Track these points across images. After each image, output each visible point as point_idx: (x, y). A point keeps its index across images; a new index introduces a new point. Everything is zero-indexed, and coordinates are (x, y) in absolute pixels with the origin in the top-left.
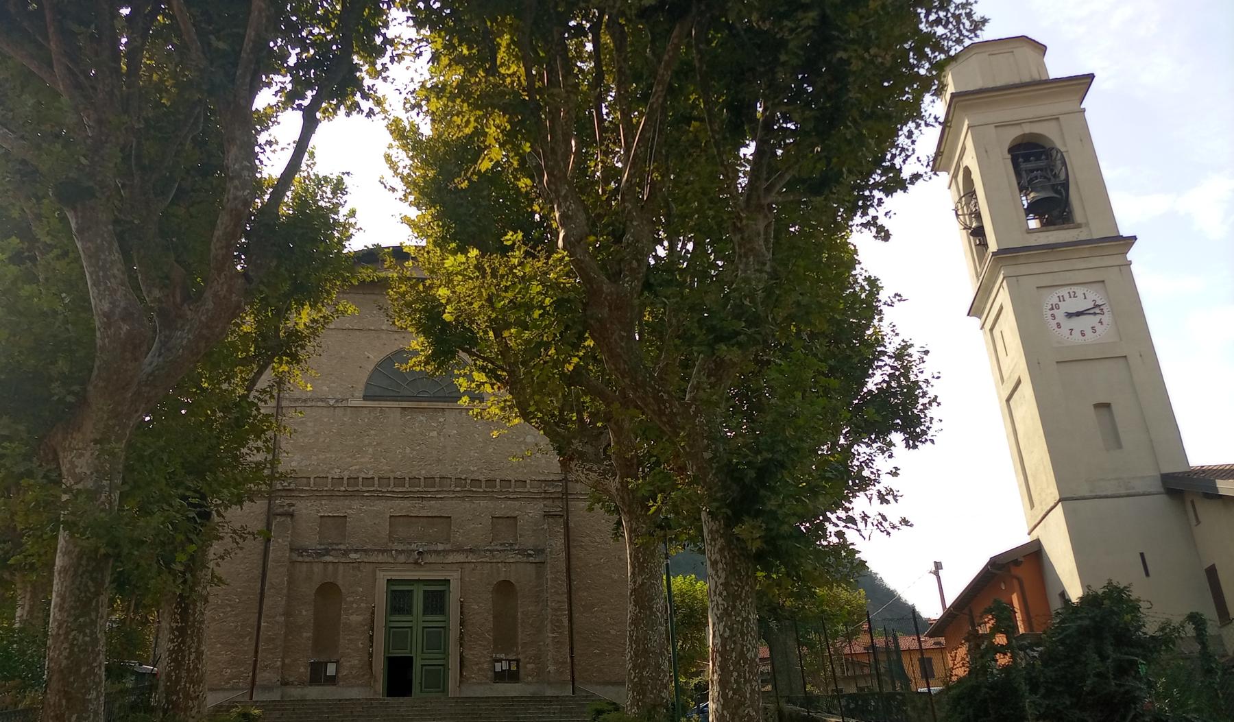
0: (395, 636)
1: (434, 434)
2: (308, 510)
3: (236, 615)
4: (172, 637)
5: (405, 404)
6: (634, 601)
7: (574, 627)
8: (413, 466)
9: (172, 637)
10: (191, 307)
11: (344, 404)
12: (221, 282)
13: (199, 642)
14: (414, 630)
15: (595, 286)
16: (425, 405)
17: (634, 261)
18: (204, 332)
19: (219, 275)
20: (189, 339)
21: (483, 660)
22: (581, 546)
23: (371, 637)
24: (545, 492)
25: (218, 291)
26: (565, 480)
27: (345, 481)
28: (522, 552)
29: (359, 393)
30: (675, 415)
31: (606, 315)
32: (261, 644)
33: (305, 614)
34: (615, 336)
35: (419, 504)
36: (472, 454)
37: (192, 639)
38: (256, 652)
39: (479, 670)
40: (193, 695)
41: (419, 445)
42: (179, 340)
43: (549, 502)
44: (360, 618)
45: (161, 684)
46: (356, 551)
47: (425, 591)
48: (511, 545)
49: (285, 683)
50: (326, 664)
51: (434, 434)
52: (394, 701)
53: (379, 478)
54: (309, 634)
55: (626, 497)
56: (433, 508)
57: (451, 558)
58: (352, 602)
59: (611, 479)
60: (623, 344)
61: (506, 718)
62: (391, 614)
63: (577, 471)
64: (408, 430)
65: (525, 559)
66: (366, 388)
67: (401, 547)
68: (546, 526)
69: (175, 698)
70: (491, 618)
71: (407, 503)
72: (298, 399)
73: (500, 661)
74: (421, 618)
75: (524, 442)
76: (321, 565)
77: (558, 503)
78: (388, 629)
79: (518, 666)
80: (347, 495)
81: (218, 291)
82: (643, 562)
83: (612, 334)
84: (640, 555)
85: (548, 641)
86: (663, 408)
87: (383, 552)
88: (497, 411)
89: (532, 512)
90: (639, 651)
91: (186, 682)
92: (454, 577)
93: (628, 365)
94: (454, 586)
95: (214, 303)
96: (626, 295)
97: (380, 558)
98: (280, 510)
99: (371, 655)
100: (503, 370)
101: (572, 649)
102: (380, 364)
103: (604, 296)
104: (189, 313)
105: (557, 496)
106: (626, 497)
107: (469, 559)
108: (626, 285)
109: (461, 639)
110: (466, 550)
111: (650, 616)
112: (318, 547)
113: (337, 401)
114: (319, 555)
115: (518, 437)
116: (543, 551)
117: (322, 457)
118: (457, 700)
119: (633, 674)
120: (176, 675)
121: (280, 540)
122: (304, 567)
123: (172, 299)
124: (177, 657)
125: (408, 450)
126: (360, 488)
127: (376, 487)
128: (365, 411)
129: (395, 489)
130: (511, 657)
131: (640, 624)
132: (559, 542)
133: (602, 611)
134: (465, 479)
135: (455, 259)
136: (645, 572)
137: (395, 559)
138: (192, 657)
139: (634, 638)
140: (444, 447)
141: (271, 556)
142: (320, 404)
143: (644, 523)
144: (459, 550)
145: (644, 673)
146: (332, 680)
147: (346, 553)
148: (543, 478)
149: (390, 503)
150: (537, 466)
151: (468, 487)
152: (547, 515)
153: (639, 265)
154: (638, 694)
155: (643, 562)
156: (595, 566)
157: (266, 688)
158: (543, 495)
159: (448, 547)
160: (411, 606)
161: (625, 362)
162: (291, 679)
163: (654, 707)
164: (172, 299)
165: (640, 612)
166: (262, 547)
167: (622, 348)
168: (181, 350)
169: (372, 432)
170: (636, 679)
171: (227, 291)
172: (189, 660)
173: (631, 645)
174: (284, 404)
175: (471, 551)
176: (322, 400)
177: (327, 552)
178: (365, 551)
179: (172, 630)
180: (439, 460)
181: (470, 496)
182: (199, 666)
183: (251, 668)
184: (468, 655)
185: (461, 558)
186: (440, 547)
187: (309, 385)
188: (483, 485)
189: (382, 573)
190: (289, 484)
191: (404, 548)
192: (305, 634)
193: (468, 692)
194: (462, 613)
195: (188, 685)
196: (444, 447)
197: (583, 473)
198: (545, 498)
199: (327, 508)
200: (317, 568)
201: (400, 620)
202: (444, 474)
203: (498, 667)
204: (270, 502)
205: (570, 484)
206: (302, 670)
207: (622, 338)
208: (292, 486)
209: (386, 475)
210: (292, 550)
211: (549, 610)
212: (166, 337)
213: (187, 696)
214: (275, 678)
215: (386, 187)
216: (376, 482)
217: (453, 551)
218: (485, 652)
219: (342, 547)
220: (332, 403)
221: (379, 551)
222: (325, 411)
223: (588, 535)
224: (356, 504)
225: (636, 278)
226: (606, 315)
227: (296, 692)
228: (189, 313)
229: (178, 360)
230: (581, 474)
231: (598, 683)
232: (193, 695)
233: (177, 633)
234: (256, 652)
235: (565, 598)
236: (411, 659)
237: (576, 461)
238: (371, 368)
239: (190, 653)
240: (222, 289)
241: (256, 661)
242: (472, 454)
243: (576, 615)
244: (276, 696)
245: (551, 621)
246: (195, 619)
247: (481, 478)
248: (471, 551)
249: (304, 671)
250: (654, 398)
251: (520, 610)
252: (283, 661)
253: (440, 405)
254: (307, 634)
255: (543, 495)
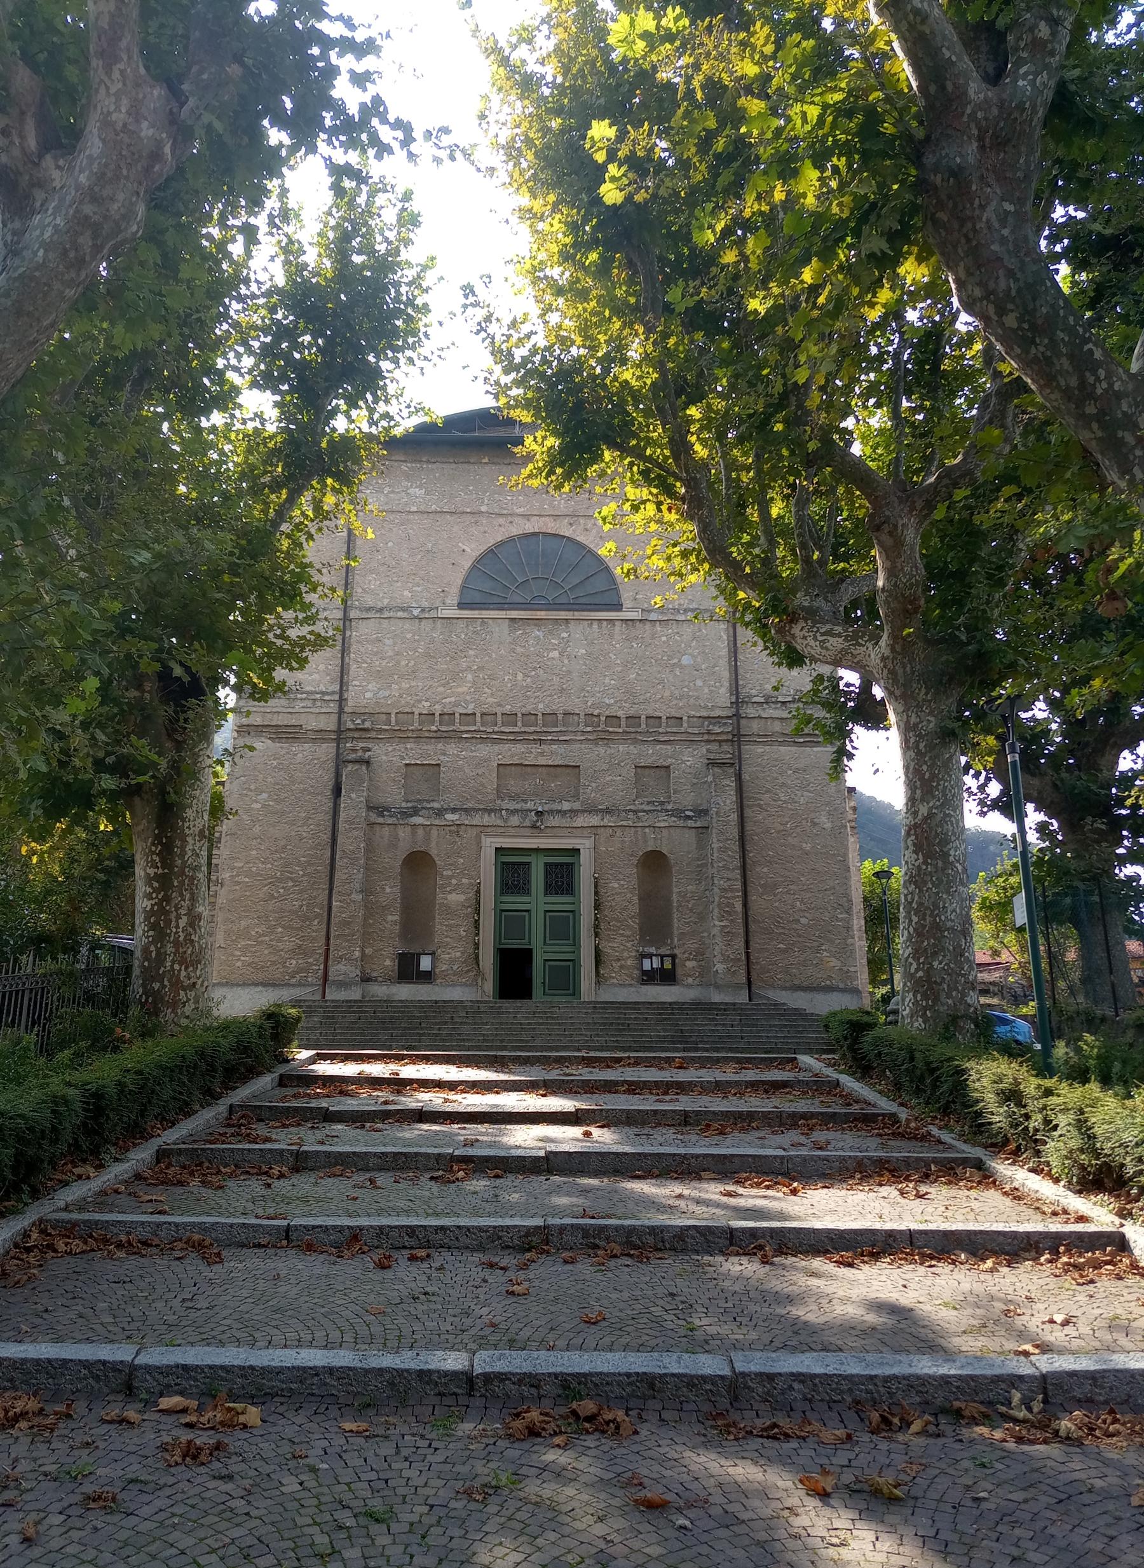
0: (508, 922)
1: (555, 654)
2: (385, 754)
3: (300, 892)
4: (149, 890)
5: (514, 614)
6: (915, 845)
7: (750, 913)
8: (528, 697)
9: (149, 890)
10: (61, 162)
11: (433, 614)
12: (113, 90)
13: (193, 899)
14: (533, 914)
15: (950, 87)
16: (542, 614)
17: (1043, 23)
18: (88, 209)
19: (109, 73)
20: (56, 226)
21: (625, 954)
22: (759, 806)
23: (477, 922)
24: (709, 733)
25: (109, 113)
26: (737, 716)
27: (437, 718)
28: (678, 813)
29: (453, 599)
30: (1118, 396)
31: (971, 159)
32: (333, 928)
33: (391, 890)
34: (989, 214)
35: (536, 749)
36: (607, 680)
37: (181, 895)
38: (328, 939)
39: (621, 967)
40: (187, 983)
41: (535, 669)
42: (38, 232)
43: (714, 747)
44: (461, 898)
45: (136, 963)
46: (454, 810)
47: (546, 864)
48: (662, 803)
49: (366, 979)
50: (419, 955)
51: (555, 654)
52: (508, 1005)
53: (483, 714)
54: (396, 918)
55: (900, 671)
56: (556, 754)
57: (580, 821)
58: (450, 877)
59: (869, 645)
60: (1006, 232)
61: (665, 1030)
62: (502, 893)
63: (805, 638)
64: (519, 650)
65: (681, 823)
66: (462, 593)
67: (513, 806)
68: (710, 779)
69: (156, 986)
70: (636, 899)
71: (520, 748)
72: (369, 609)
73: (650, 956)
74: (542, 899)
75: (679, 665)
76: (408, 829)
77: (726, 747)
78: (500, 913)
79: (673, 964)
80: (439, 736)
81: (109, 113)
82: (931, 779)
83: (982, 207)
84: (925, 768)
85: (715, 931)
86: (1091, 380)
87: (489, 811)
88: (661, 564)
89: (690, 759)
90: (924, 926)
91: (173, 962)
92: (585, 845)
93: (1017, 280)
94: (586, 859)
95: (103, 141)
96: (1021, 108)
97: (486, 820)
98: (352, 756)
99: (477, 946)
100: (677, 478)
101: (747, 942)
102: (480, 560)
103: (969, 111)
104: (56, 174)
105: (724, 737)
106: (900, 671)
107: (606, 822)
108: (1021, 83)
109: (596, 926)
110: (601, 811)
111: (943, 869)
112: (404, 805)
113: (423, 610)
114: (405, 814)
115: (670, 658)
116: (706, 812)
117: (404, 685)
118: (598, 1006)
119: (914, 966)
120: (158, 950)
121: (353, 796)
122: (386, 831)
123: (17, 141)
124: (159, 921)
125: (520, 676)
126: (457, 727)
127: (478, 726)
128: (461, 624)
129: (503, 729)
130: (663, 951)
131: (925, 883)
132: (729, 800)
133: (788, 893)
134: (598, 716)
135: (632, 23)
136: (934, 797)
137: (506, 821)
138: (183, 922)
139: (914, 905)
140: (569, 672)
141: (342, 815)
142: (400, 614)
143: (931, 713)
144: (592, 810)
145: (935, 964)
146: (427, 977)
147: (440, 813)
148: (705, 714)
149: (497, 748)
150: (698, 698)
151: (602, 726)
152: (712, 763)
153: (1054, 34)
154: (925, 997)
155: (931, 779)
156: (778, 832)
157: (342, 985)
158: (706, 737)
159: (577, 806)
160: (528, 882)
161: (1011, 274)
162: (375, 974)
163: (954, 1019)
164: (17, 141)
165: (925, 863)
166: (331, 805)
167: (1003, 241)
168: (41, 253)
169: (471, 652)
170: (920, 974)
171: (129, 113)
172: (177, 927)
173: (908, 916)
174: (353, 614)
175: (608, 811)
176: (403, 609)
177: (416, 812)
178: (466, 810)
179: (149, 880)
180: (562, 691)
181: (605, 738)
182: (195, 938)
183: (322, 959)
184: (607, 948)
185: (595, 820)
186: (566, 806)
187: (369, 530)
188: (623, 722)
189: (489, 840)
190: (363, 721)
191: (518, 806)
192: (390, 918)
193: (606, 995)
194: (596, 893)
195: (177, 967)
196: (569, 672)
197: (815, 639)
198: (708, 741)
199: (414, 753)
200: (403, 833)
201: (515, 901)
202: (569, 709)
203: (647, 964)
204: (338, 748)
205: (743, 722)
206: (388, 963)
207: (1004, 217)
208: (367, 725)
209: (493, 710)
210: (369, 808)
211: (716, 890)
212: (14, 233)
213: (177, 984)
214: (353, 972)
215: (479, 170)
216: (478, 719)
217: (583, 811)
218: (629, 945)
219: (436, 805)
220: (416, 612)
221: (485, 810)
222: (408, 625)
223: (768, 791)
224: (452, 749)
225: (1046, 67)
226: (971, 159)
227: (380, 991)
228: (56, 174)
229: (37, 274)
230: (812, 643)
231: (785, 988)
232: (187, 983)
233: (156, 885)
234: (328, 939)
235: (737, 874)
236: (529, 952)
237: (801, 623)
238: (467, 565)
239: (178, 917)
240: (118, 109)
241: (327, 950)
242: (607, 680)
243: (753, 898)
244: (355, 994)
245: (719, 906)
246: (184, 862)
247: (620, 713)
248: (608, 811)
249: (389, 963)
250: (1071, 357)
251: (675, 890)
252: (363, 951)
253: (563, 615)
254: (393, 917)
255: (706, 737)
